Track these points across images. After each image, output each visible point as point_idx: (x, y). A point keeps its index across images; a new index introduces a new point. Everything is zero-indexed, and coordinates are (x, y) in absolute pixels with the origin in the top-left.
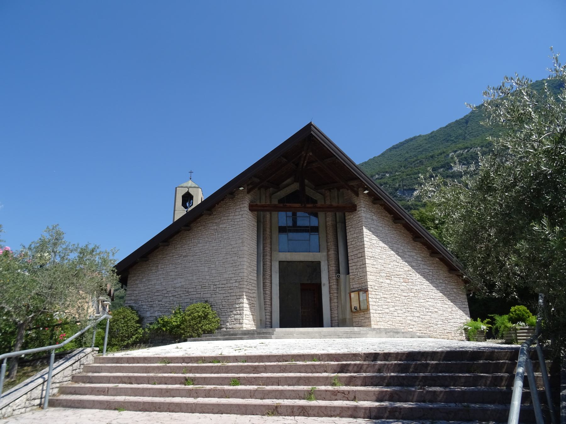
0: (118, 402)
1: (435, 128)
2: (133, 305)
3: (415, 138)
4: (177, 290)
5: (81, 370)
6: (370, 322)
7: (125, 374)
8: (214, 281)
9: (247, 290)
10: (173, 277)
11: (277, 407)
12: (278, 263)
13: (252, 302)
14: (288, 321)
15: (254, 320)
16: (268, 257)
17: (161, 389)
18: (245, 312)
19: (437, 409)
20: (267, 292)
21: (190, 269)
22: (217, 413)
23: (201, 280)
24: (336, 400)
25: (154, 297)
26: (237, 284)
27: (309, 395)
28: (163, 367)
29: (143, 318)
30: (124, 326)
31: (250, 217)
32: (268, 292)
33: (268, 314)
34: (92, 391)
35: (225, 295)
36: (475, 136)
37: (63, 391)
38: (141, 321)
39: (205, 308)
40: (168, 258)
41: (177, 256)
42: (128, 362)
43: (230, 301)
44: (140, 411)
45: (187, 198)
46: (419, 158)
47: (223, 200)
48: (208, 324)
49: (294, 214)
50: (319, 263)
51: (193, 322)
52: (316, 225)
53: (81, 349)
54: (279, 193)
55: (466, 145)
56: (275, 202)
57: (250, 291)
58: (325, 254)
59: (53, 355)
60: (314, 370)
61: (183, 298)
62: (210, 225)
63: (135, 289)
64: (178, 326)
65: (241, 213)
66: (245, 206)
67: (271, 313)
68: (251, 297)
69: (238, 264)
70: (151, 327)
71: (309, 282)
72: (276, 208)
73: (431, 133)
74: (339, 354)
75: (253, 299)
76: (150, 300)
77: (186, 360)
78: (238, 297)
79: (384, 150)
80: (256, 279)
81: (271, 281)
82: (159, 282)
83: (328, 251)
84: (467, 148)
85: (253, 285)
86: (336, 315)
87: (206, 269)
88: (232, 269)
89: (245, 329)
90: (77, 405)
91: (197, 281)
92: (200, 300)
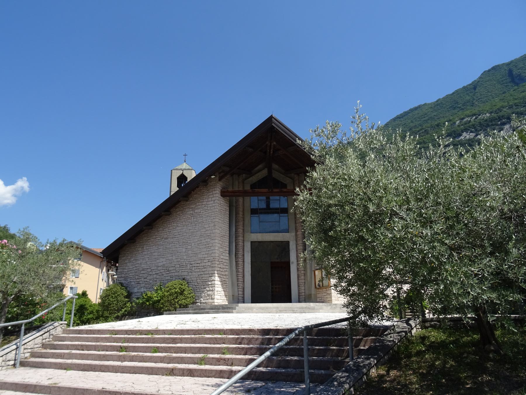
0: (67, 364)
1: (442, 96)
2: (123, 282)
3: (419, 107)
4: (159, 268)
5: (51, 339)
6: (331, 297)
7: (80, 343)
8: (190, 260)
9: (219, 269)
10: (156, 257)
11: (173, 369)
12: (249, 244)
13: (224, 279)
14: (258, 297)
15: (226, 296)
16: (241, 238)
17: (100, 355)
18: (216, 289)
19: (281, 373)
20: (239, 270)
21: (171, 250)
22: (133, 373)
23: (179, 260)
24: (219, 365)
25: (141, 275)
26: (209, 264)
27: (200, 361)
28: (109, 338)
29: (132, 293)
30: (115, 301)
31: (222, 202)
32: (241, 270)
33: (240, 290)
34: (54, 356)
35: (199, 273)
36: (484, 102)
37: (33, 355)
38: (129, 296)
39: (182, 285)
40: (152, 240)
41: (159, 238)
42: (86, 334)
43: (203, 278)
44: (81, 370)
45: (182, 178)
46: (424, 127)
47: (198, 187)
48: (184, 299)
49: (268, 198)
50: (288, 243)
51: (171, 298)
52: (286, 207)
53: (53, 322)
54: (251, 179)
55: (474, 112)
56: (248, 188)
57: (221, 270)
58: (294, 234)
59: (23, 328)
60: (216, 342)
61: (165, 275)
62: (187, 210)
63: (124, 267)
64: (159, 301)
65: (213, 199)
66: (217, 191)
67: (244, 289)
68: (223, 275)
69: (210, 245)
70: (137, 301)
71: (279, 260)
72: (245, 194)
73: (437, 101)
74: (239, 330)
75: (224, 277)
76: (137, 277)
77: (128, 333)
78: (211, 275)
79: (388, 121)
80: (228, 258)
81: (244, 260)
82: (144, 261)
83: (296, 231)
84: (475, 115)
85: (225, 264)
86: (303, 291)
87: (184, 250)
88: (205, 250)
89: (216, 304)
90: (40, 366)
91: (176, 261)
92: (178, 277)
